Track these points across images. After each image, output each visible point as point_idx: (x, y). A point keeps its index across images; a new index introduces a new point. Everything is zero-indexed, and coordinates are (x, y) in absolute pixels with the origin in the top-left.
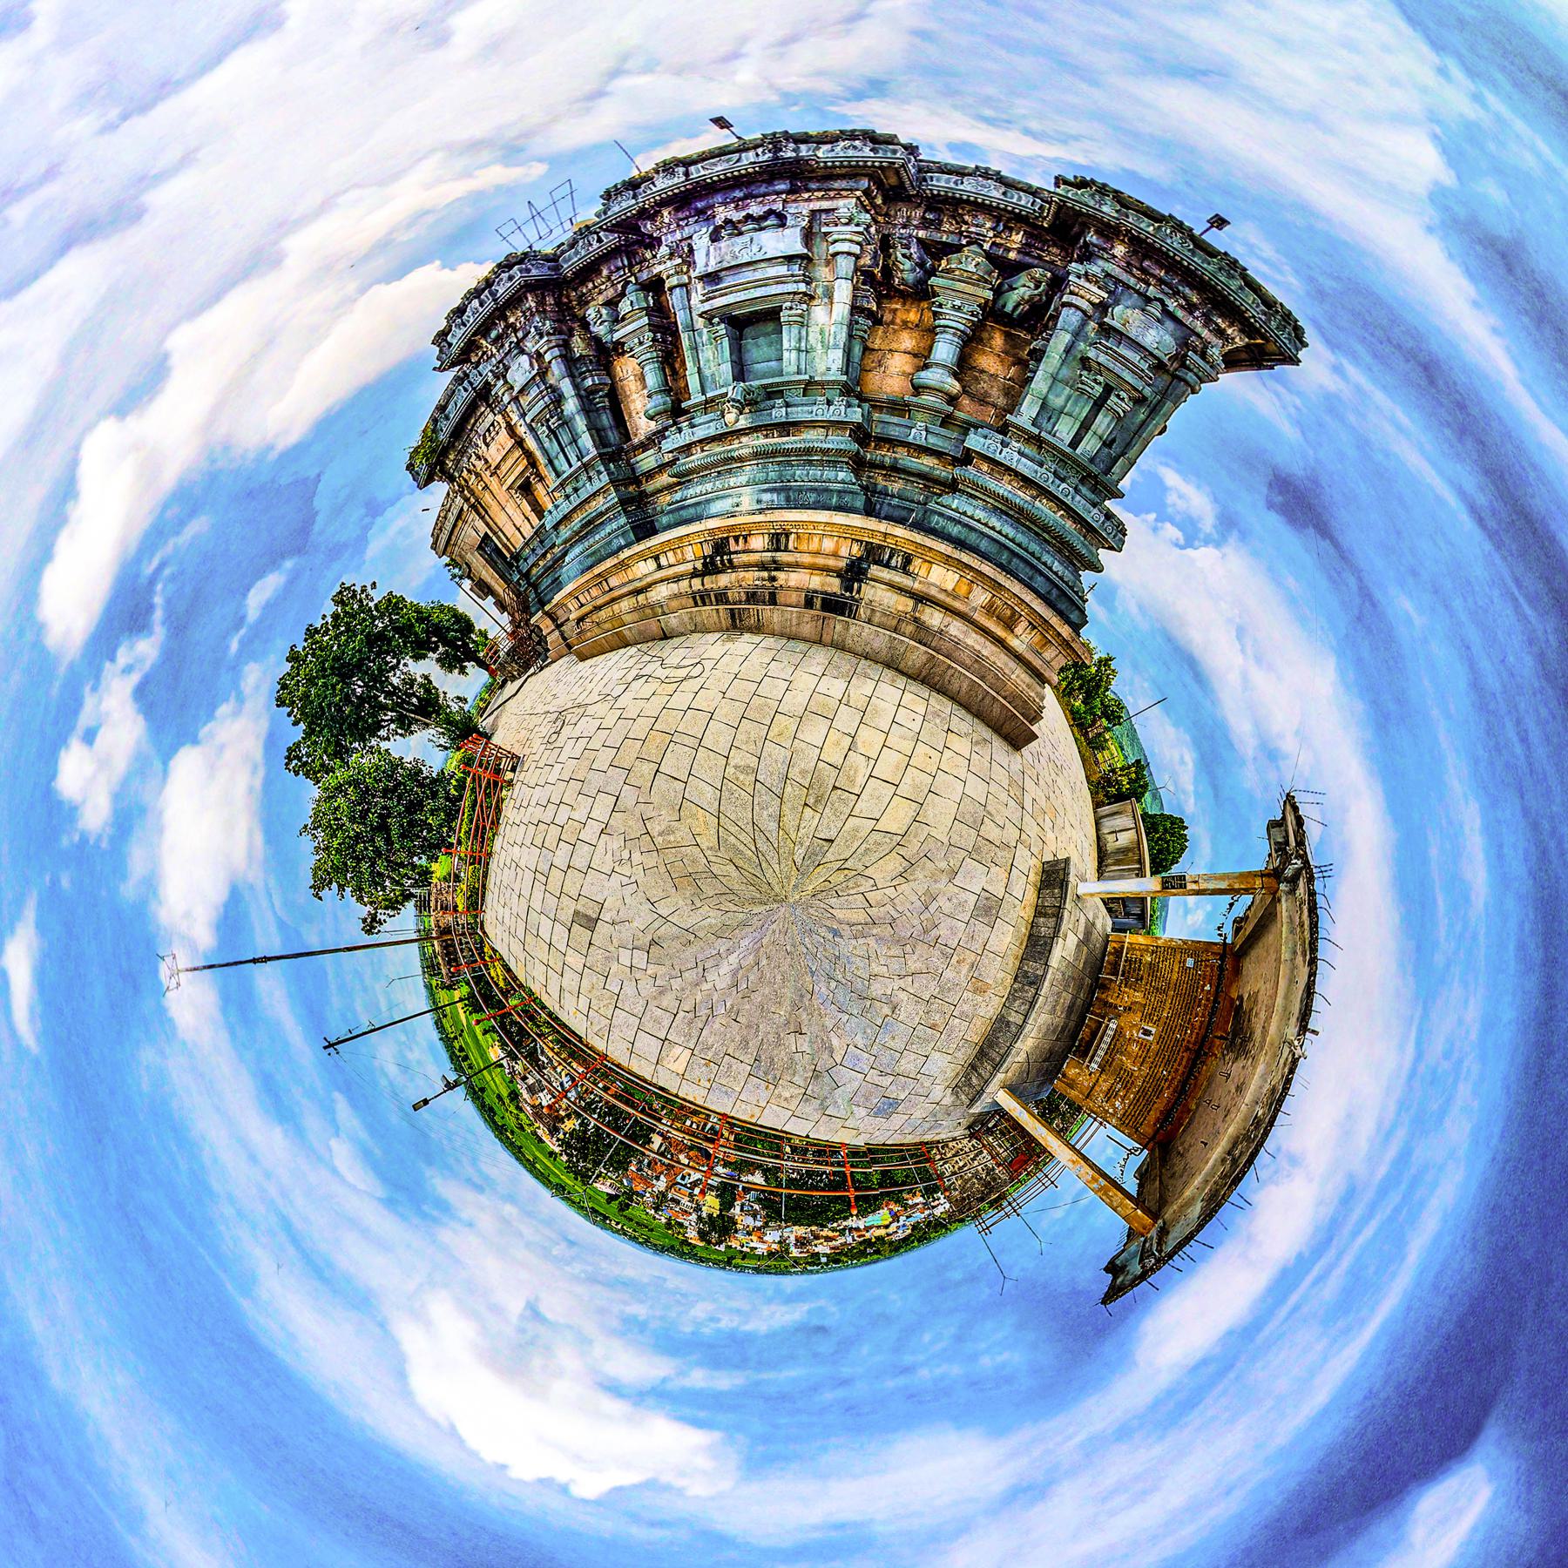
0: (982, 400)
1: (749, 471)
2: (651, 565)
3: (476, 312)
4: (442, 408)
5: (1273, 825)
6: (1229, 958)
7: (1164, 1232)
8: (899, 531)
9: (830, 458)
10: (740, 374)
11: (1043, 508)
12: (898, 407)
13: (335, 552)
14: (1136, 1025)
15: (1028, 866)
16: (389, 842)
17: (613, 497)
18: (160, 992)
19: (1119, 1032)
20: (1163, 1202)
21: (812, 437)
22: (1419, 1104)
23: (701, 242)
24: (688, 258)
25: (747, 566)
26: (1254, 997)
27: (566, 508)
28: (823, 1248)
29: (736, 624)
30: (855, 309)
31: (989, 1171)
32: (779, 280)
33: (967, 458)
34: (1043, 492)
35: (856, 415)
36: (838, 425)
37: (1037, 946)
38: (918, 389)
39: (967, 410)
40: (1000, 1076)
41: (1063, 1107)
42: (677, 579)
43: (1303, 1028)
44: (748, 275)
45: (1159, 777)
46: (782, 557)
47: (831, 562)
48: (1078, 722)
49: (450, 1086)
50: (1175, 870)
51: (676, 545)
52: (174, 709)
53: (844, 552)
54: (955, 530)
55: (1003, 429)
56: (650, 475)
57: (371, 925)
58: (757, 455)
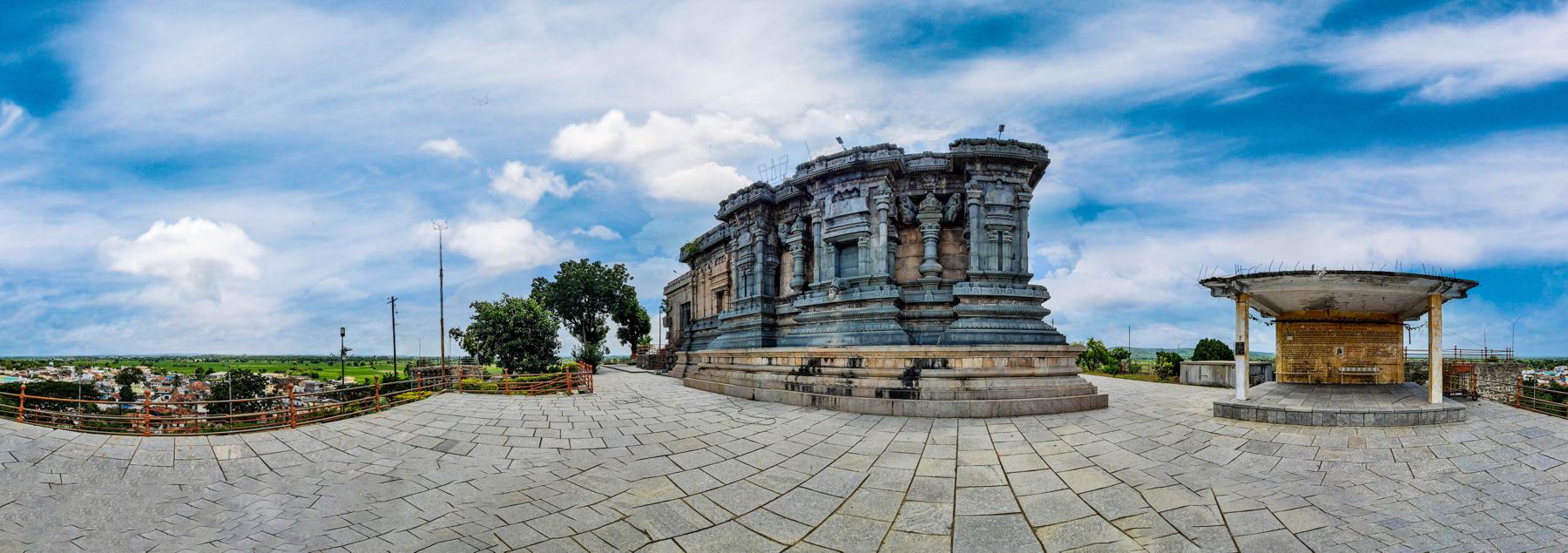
1: (839, 325)
2: (765, 361)
3: (741, 202)
4: (708, 235)
5: (1213, 294)
6: (1285, 320)
7: (1432, 289)
8: (934, 348)
9: (884, 318)
10: (838, 274)
11: (1005, 305)
12: (916, 285)
13: (634, 252)
14: (1340, 358)
15: (1215, 424)
16: (506, 340)
17: (759, 320)
19: (1346, 365)
20: (1421, 299)
23: (828, 201)
25: (830, 375)
26: (1303, 301)
27: (733, 314)
28: (51, 369)
29: (815, 403)
30: (890, 238)
31: (1484, 376)
32: (857, 224)
33: (957, 300)
35: (896, 294)
37: (1294, 419)
38: (923, 274)
39: (948, 276)
40: (1424, 408)
42: (779, 373)
43: (1312, 273)
44: (845, 222)
45: (1170, 345)
46: (855, 371)
47: (893, 372)
48: (1115, 372)
49: (344, 351)
50: (1232, 347)
51: (788, 356)
53: (901, 365)
54: (967, 338)
55: (968, 280)
56: (783, 316)
57: (455, 333)
58: (843, 316)
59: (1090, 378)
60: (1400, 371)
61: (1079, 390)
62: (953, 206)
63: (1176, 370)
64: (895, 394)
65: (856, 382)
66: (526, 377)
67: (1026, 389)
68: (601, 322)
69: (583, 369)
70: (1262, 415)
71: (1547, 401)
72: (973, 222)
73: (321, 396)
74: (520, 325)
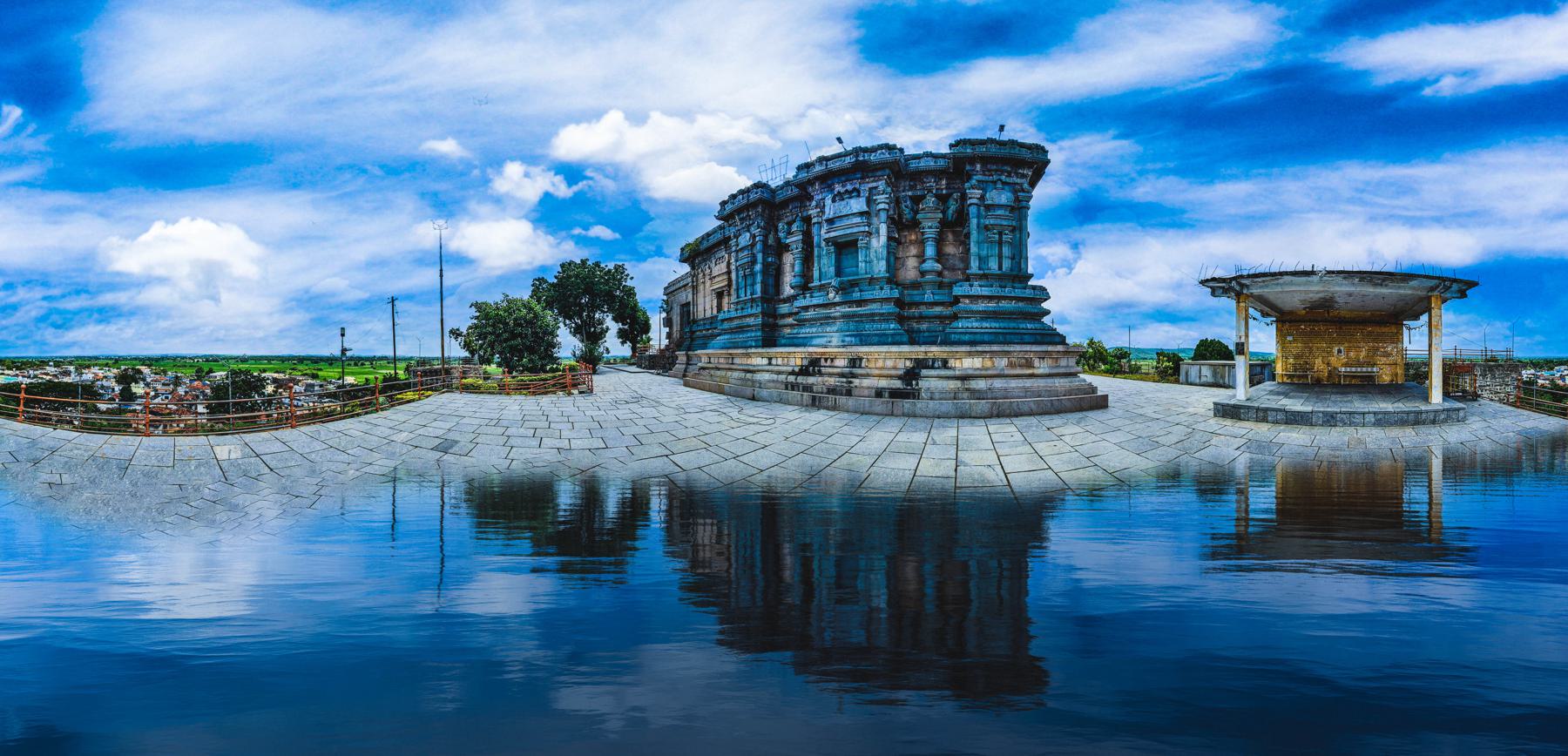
0: (953, 269)
1: (839, 324)
2: (765, 361)
3: (741, 201)
4: (708, 235)
6: (1286, 320)
7: (1432, 289)
8: (934, 348)
9: (885, 318)
10: (839, 273)
11: (1004, 304)
12: (916, 285)
14: (1337, 358)
15: (1215, 424)
16: (506, 340)
18: (433, 218)
19: (1346, 365)
20: (1421, 299)
21: (874, 307)
22: (1328, 203)
23: (828, 202)
24: (821, 207)
25: (830, 375)
27: (733, 314)
29: (815, 403)
30: (890, 238)
31: (1484, 376)
33: (957, 300)
34: (1000, 298)
35: (896, 294)
36: (887, 300)
37: (1294, 419)
38: (923, 273)
39: (948, 276)
41: (1412, 372)
42: (779, 373)
44: (846, 222)
47: (893, 372)
48: (1115, 372)
49: (344, 351)
50: (1232, 348)
52: (549, 214)
53: (901, 364)
54: (966, 338)
55: (967, 279)
57: (455, 333)
58: (843, 316)
59: (1089, 378)
60: (1400, 371)
61: (1079, 390)
62: (953, 207)
63: (1176, 370)
64: (895, 394)
65: (856, 382)
66: (526, 377)
67: (1026, 390)
68: (601, 322)
69: (581, 367)
70: (1262, 415)
71: (1547, 401)
72: (974, 221)
73: (321, 396)
74: (520, 325)
